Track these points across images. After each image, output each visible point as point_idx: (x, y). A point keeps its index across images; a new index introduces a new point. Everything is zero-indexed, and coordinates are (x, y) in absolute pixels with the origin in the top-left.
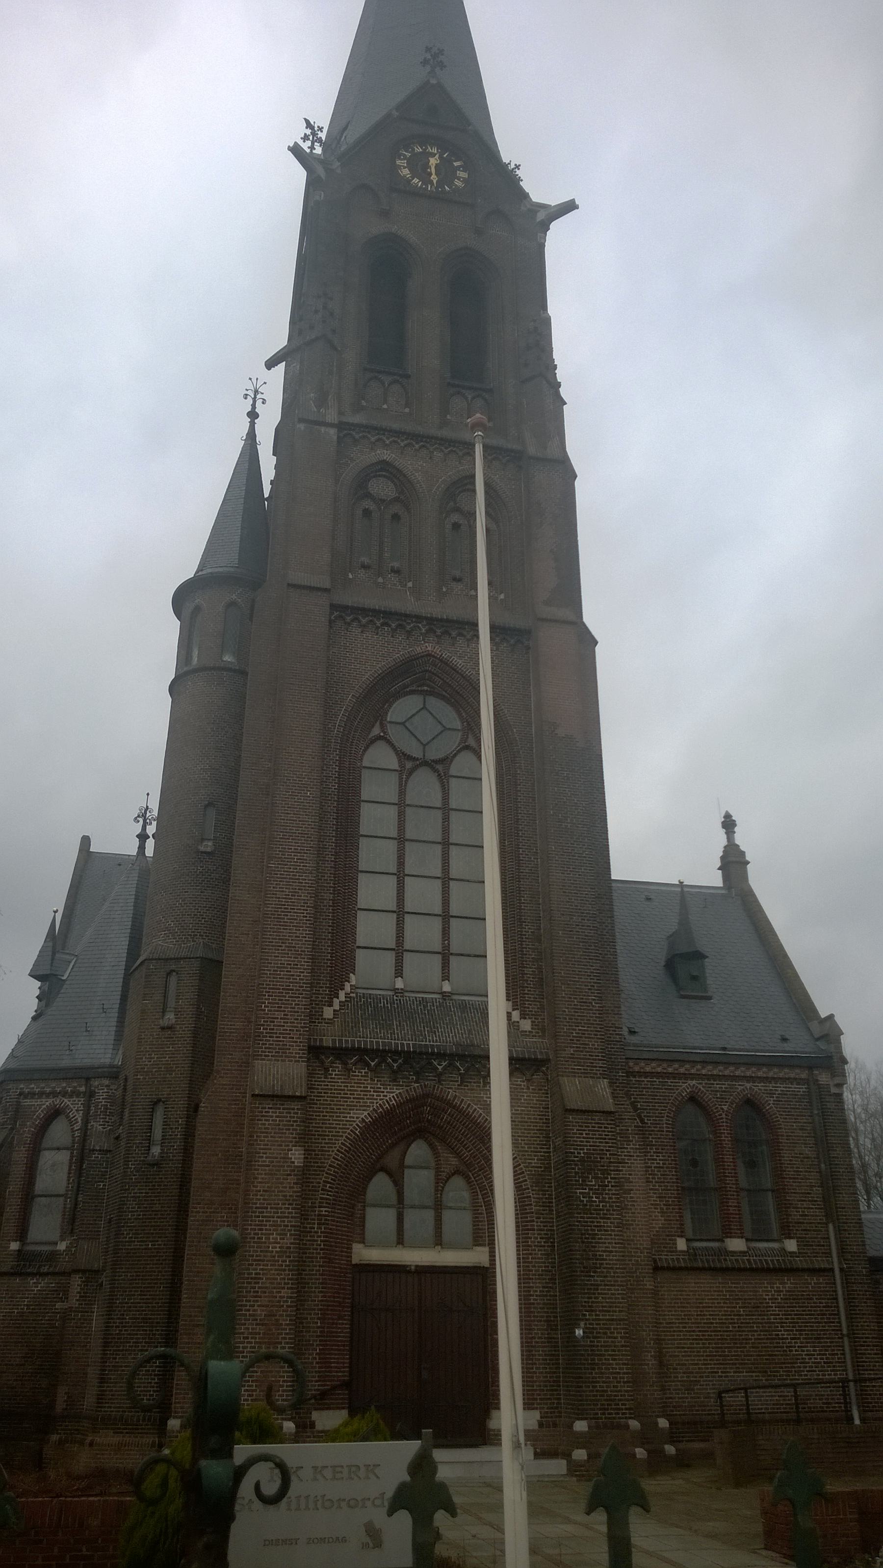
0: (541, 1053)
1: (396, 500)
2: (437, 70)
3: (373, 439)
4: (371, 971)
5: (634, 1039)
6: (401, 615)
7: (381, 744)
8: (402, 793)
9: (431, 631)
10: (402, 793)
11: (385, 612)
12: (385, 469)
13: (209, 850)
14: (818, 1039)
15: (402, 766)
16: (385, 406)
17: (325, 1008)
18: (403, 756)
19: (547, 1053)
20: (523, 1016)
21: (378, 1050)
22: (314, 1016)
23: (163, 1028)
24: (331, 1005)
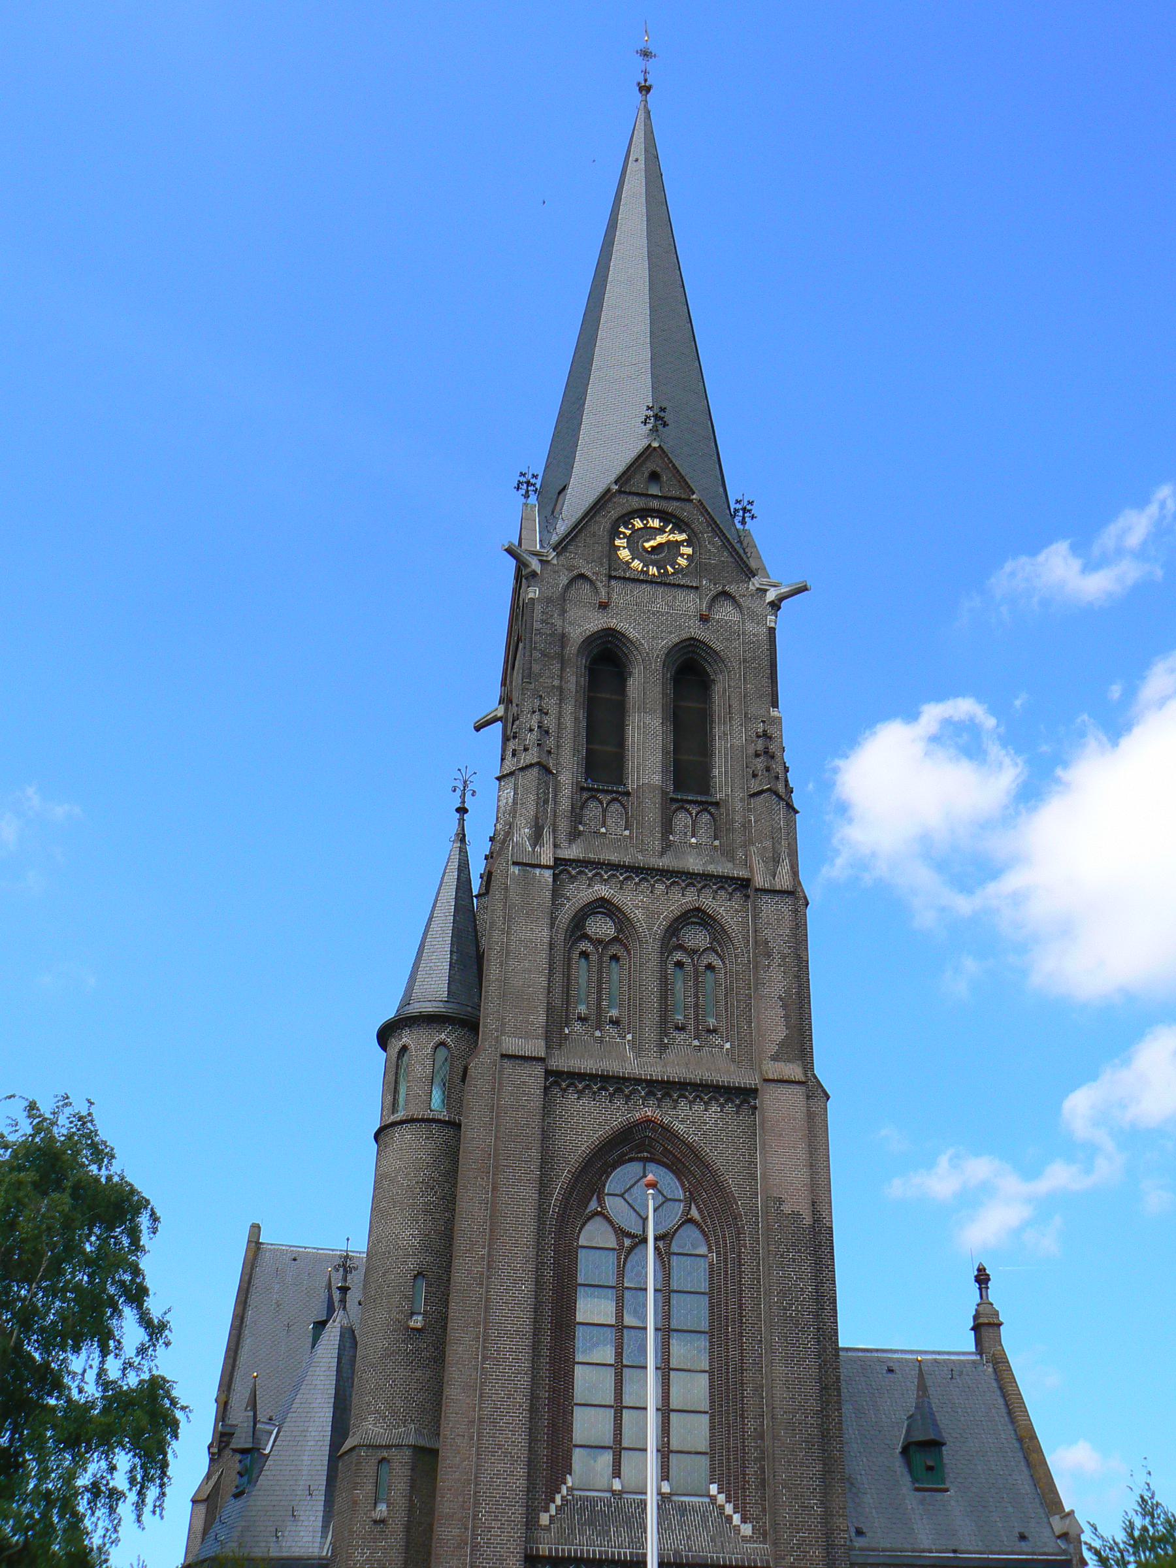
0: (761, 1560)
1: (615, 939)
2: (660, 427)
3: (590, 875)
4: (589, 1472)
5: (859, 1542)
6: (619, 1078)
7: (598, 1219)
8: (621, 1274)
9: (650, 1094)
10: (621, 1274)
11: (602, 1076)
12: (603, 906)
13: (419, 1325)
14: (1059, 1537)
15: (621, 1245)
16: (603, 830)
17: (541, 1514)
18: (621, 1233)
19: (768, 1561)
20: (744, 1521)
21: (594, 1559)
22: (531, 1523)
23: (375, 1522)
24: (547, 1511)
